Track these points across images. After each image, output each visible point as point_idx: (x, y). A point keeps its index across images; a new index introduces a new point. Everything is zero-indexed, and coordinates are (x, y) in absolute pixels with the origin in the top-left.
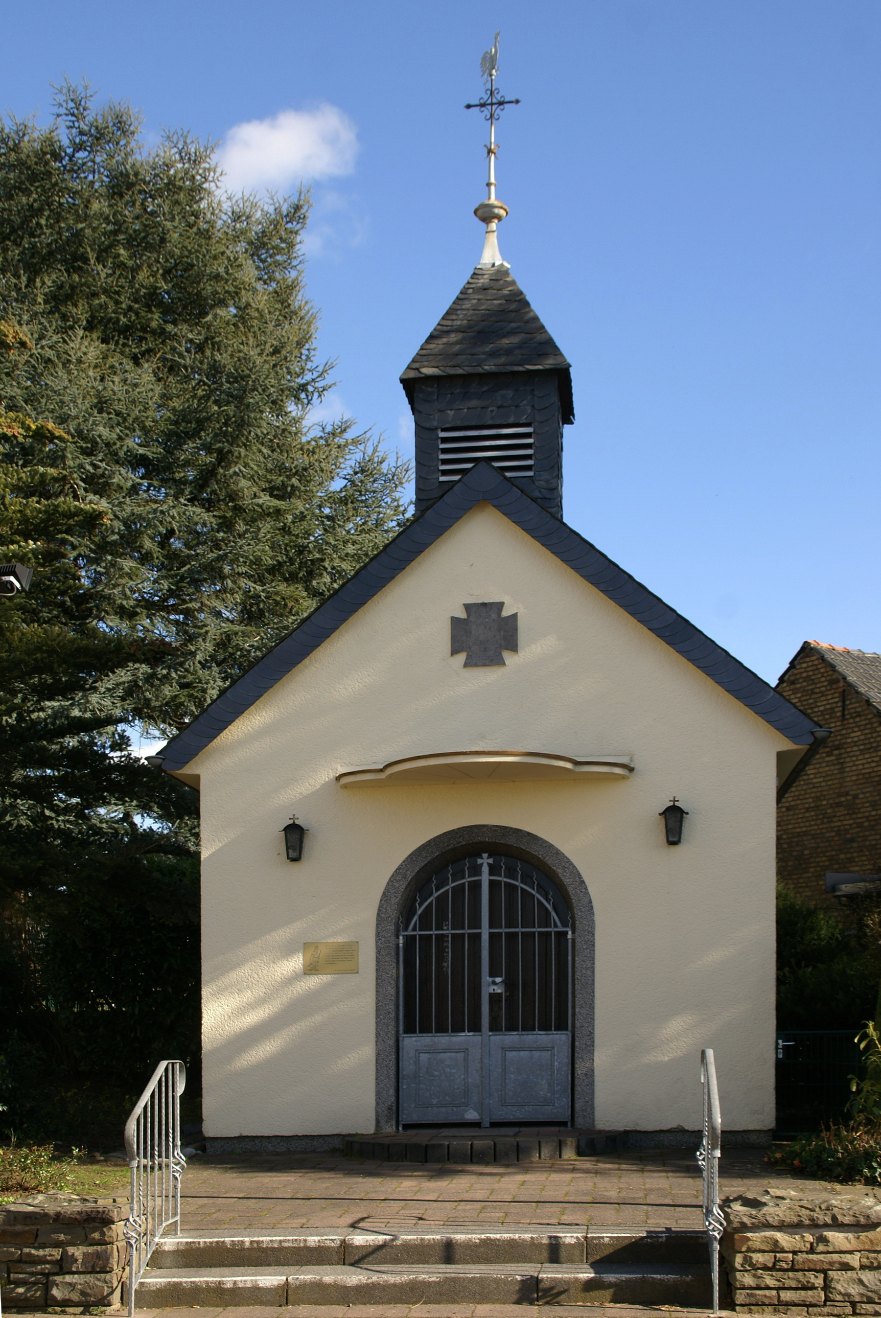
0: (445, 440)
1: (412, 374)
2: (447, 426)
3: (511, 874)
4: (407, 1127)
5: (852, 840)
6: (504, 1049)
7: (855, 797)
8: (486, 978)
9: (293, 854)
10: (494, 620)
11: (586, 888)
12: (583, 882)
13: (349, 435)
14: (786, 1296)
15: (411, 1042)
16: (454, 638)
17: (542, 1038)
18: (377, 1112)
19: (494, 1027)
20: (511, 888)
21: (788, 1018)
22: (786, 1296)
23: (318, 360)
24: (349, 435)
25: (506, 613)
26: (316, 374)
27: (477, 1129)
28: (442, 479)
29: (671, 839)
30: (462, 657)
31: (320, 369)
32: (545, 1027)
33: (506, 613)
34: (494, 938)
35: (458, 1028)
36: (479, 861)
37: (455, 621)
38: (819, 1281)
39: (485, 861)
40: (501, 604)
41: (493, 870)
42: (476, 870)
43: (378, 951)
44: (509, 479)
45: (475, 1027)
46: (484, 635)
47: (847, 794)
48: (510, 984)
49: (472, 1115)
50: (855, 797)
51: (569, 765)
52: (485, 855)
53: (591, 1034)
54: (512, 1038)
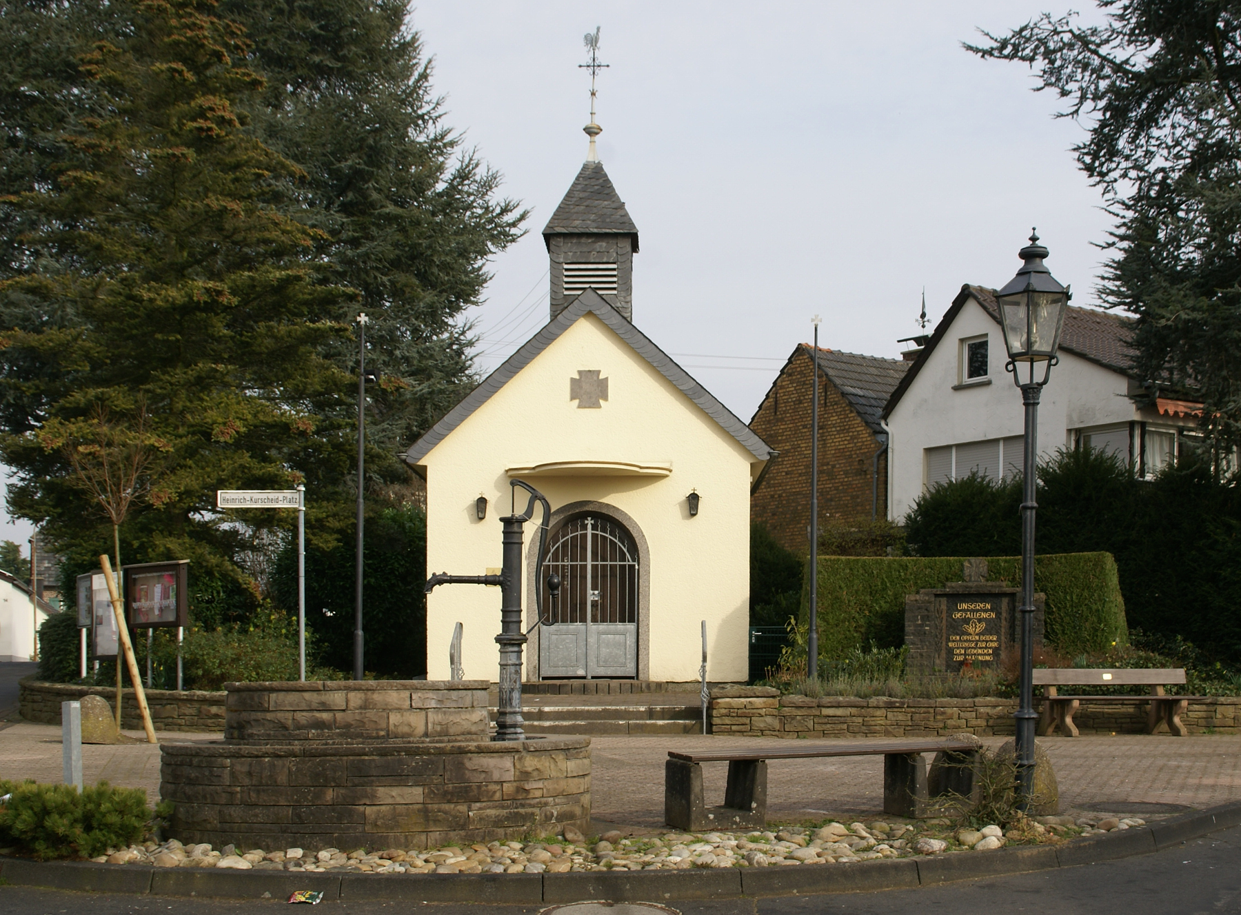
0: (567, 270)
1: (549, 231)
3: (604, 530)
4: (544, 678)
5: (831, 500)
6: (599, 633)
7: (834, 466)
8: (590, 592)
13: (447, 139)
14: (734, 728)
16: (572, 390)
17: (620, 626)
19: (594, 620)
20: (604, 538)
21: (756, 619)
22: (734, 728)
23: (432, 96)
24: (447, 139)
25: (601, 377)
26: (432, 106)
28: (566, 293)
30: (576, 402)
31: (435, 101)
32: (622, 620)
33: (601, 377)
34: (594, 568)
35: (573, 620)
37: (573, 380)
38: (748, 721)
39: (589, 522)
41: (594, 527)
42: (584, 527)
44: (600, 296)
45: (583, 620)
46: (589, 390)
47: (828, 464)
48: (603, 596)
49: (581, 672)
50: (834, 466)
53: (648, 625)
54: (603, 627)
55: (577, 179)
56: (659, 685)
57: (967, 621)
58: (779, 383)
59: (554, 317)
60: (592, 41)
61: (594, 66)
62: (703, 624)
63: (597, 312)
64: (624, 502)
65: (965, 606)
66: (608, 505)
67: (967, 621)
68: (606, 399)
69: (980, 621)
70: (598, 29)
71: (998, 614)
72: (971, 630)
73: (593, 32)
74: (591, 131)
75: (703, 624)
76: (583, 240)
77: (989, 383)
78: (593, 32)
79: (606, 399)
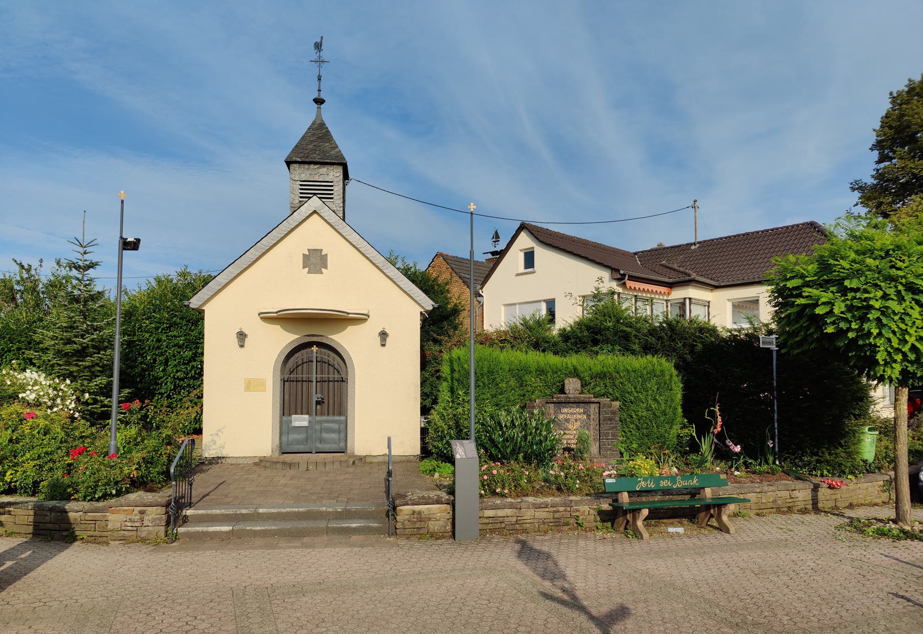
55: (309, 129)
56: (362, 459)
57: (567, 420)
59: (726, 504)
60: (318, 46)
62: (389, 439)
64: (343, 339)
65: (565, 410)
67: (567, 420)
68: (326, 268)
69: (576, 420)
71: (589, 416)
72: (570, 427)
73: (319, 41)
74: (319, 101)
75: (389, 439)
76: (312, 166)
77: (534, 272)
78: (319, 41)
79: (326, 268)
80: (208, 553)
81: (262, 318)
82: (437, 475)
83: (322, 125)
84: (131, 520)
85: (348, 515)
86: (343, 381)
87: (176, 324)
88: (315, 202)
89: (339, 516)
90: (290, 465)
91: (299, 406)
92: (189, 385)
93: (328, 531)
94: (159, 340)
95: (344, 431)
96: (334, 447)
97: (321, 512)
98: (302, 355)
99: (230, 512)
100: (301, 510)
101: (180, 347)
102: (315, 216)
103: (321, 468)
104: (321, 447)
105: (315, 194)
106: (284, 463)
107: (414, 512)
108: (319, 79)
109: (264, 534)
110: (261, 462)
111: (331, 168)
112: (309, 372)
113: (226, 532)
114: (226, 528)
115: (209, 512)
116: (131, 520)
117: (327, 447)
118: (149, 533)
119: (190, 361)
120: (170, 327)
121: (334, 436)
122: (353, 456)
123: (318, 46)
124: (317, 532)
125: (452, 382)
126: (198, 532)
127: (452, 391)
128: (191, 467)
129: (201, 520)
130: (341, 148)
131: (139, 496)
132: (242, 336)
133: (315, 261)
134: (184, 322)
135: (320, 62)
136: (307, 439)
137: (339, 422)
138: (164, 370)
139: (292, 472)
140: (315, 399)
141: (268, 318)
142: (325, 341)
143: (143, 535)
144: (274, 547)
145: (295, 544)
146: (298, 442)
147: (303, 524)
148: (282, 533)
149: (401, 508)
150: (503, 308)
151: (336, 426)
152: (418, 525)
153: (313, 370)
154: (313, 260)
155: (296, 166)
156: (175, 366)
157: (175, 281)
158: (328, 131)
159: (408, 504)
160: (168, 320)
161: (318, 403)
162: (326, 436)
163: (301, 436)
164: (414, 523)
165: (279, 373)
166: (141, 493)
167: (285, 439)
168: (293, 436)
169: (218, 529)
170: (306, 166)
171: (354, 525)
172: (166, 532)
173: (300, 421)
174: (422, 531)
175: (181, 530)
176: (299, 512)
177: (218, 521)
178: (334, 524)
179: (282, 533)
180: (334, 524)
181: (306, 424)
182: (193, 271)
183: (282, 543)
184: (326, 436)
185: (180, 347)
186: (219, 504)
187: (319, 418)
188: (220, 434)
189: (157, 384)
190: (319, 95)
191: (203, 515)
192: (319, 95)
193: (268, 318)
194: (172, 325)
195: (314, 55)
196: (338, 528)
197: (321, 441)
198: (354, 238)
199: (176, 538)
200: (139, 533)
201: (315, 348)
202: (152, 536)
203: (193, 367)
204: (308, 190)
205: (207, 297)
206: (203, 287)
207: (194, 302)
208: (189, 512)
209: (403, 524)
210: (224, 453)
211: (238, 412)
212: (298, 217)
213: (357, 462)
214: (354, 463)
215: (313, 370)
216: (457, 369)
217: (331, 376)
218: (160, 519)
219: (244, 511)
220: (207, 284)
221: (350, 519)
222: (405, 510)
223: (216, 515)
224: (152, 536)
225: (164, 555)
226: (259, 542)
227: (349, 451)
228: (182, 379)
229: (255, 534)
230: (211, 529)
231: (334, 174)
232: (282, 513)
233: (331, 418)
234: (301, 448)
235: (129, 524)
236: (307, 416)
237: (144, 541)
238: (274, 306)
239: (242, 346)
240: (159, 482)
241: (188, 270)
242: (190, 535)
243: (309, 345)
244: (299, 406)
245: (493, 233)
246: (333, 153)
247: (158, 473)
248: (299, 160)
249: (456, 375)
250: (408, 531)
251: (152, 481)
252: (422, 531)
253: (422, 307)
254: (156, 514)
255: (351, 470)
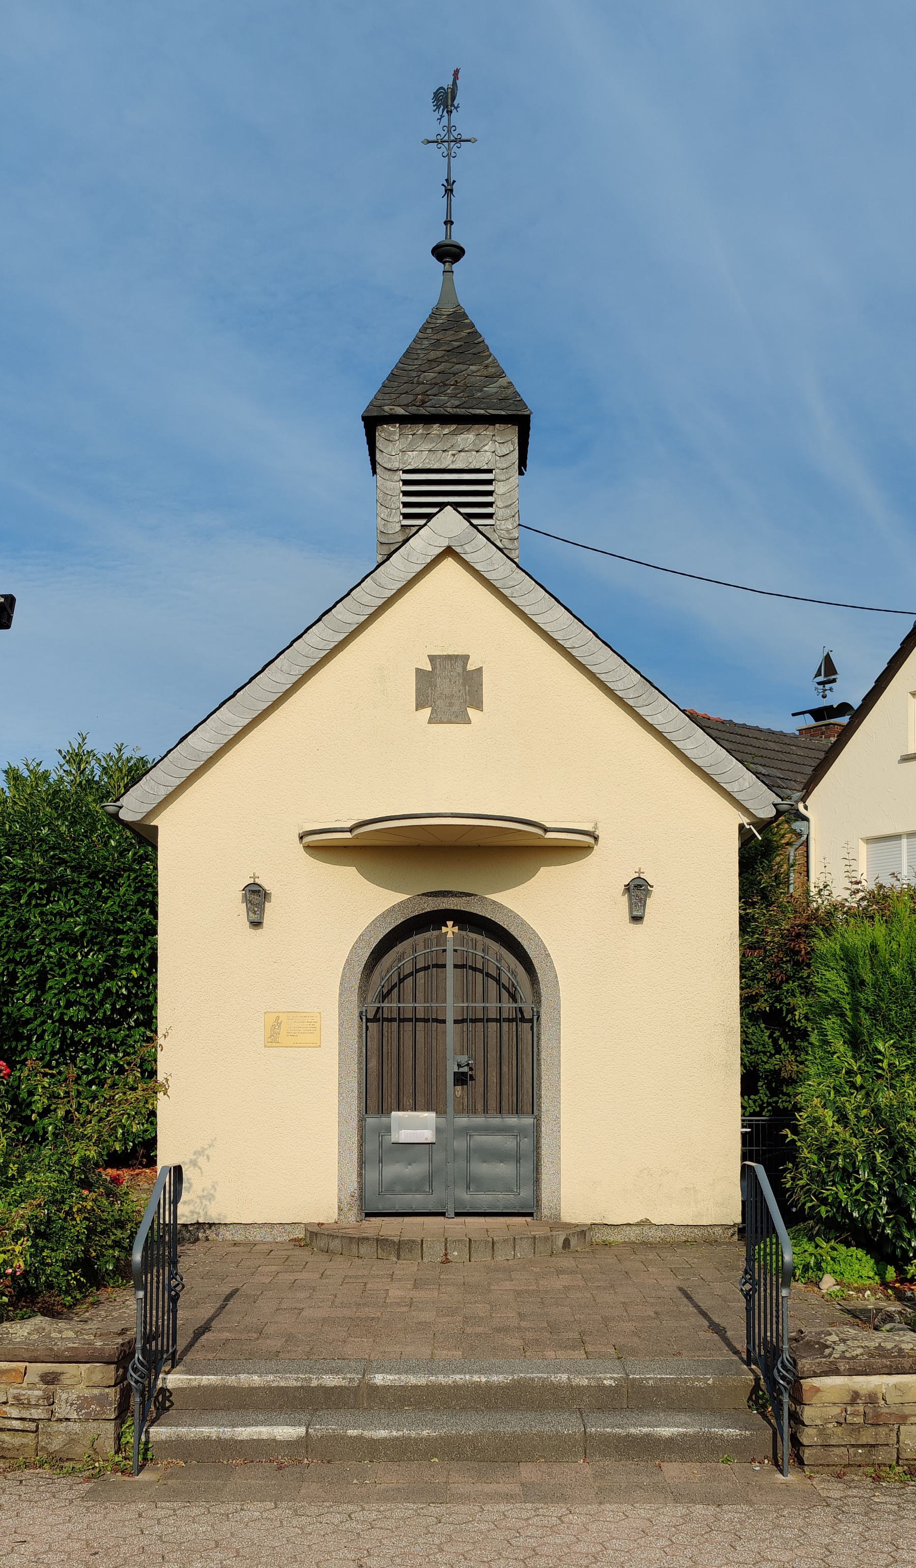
2: (409, 467)
9: (254, 917)
10: (459, 674)
11: (551, 962)
12: (548, 955)
15: (371, 1121)
18: (339, 1199)
27: (442, 1218)
29: (635, 913)
36: (444, 929)
40: (467, 657)
43: (341, 1025)
51: (540, 832)
52: (450, 923)
55: (423, 329)
56: (583, 1231)
58: (148, 916)
60: (445, 99)
61: (451, 141)
62: (794, 715)
63: (458, 550)
64: (530, 903)
66: (502, 907)
68: (479, 706)
70: (456, 73)
74: (448, 253)
75: (794, 715)
76: (436, 429)
78: (447, 82)
79: (479, 706)
80: (254, 1510)
81: (309, 848)
82: (828, 1283)
83: (458, 319)
84: (19, 1402)
85: (634, 1398)
86: (533, 1020)
87: (64, 881)
88: (448, 525)
89: (608, 1401)
90: (399, 1247)
91: (408, 1089)
92: (97, 1041)
93: (588, 1446)
94: (22, 925)
95: (531, 1157)
96: (502, 1199)
97: (555, 1389)
98: (416, 947)
99: (291, 1381)
100: (496, 1378)
101: (76, 941)
102: (449, 562)
103: (482, 1257)
104: (469, 1198)
105: (442, 506)
106: (381, 1242)
107: (855, 1396)
108: (449, 191)
109: (399, 1451)
110: (314, 1238)
111: (487, 431)
112: (436, 992)
113: (289, 1444)
114: (286, 1432)
115: (231, 1380)
116: (19, 1402)
117: (484, 1200)
118: (72, 1441)
119: (99, 979)
120: (48, 891)
121: (505, 1169)
122: (557, 1224)
123: (445, 99)
124: (557, 1450)
125: (856, 1016)
126: (207, 1441)
127: (855, 1042)
128: (171, 1240)
129: (210, 1403)
130: (512, 376)
131: (38, 1330)
132: (256, 896)
133: (450, 688)
134: (83, 879)
135: (451, 141)
136: (430, 1178)
137: (518, 1132)
138: (36, 1002)
139: (407, 1267)
140: (452, 1068)
141: (325, 847)
142: (476, 909)
143: (56, 1445)
144: (437, 1495)
145: (502, 1488)
146: (410, 1186)
147: (512, 1424)
148: (452, 1450)
149: (817, 1382)
150: (863, 848)
151: (508, 1143)
152: (867, 1437)
153: (447, 990)
154: (443, 685)
155: (393, 429)
156: (64, 990)
157: (53, 777)
158: (476, 334)
159: (836, 1372)
160: (42, 871)
161: (461, 1079)
162: (482, 1169)
163: (416, 1170)
164: (855, 1429)
165: (355, 997)
166: (39, 1320)
167: (372, 1175)
168: (393, 1170)
169: (263, 1432)
170: (420, 429)
171: (666, 1432)
172: (119, 1438)
173: (414, 1126)
174: (881, 1456)
175: (159, 1433)
176: (489, 1386)
177: (227, 1408)
178: (604, 1427)
179: (452, 1450)
180: (604, 1427)
181: (428, 1135)
182: (102, 746)
183: (462, 1483)
184: (482, 1169)
185: (76, 941)
186: (252, 1359)
187: (463, 1121)
188: (201, 1161)
189: (19, 1037)
190: (448, 234)
191: (212, 1390)
192: (448, 234)
193: (325, 847)
194: (54, 886)
195: (431, 123)
196: (618, 1438)
197: (470, 1182)
198: (556, 619)
199: (146, 1457)
200: (43, 1441)
201: (450, 929)
202: (81, 1450)
203: (108, 992)
204: (425, 496)
205: (163, 792)
206: (127, 788)
207: (132, 807)
208: (173, 1380)
209: (822, 1431)
210: (213, 1215)
211: (251, 1096)
212: (400, 567)
213: (573, 1242)
214: (567, 1243)
215: (447, 990)
216: (868, 977)
217: (493, 1005)
218: (101, 1400)
219: (330, 1380)
220: (135, 781)
221: (641, 1410)
222: (827, 1392)
223: (252, 1390)
224: (81, 1450)
225: (128, 1513)
226: (389, 1476)
227: (545, 1212)
228: (81, 1025)
229: (373, 1450)
230: (245, 1433)
231: (490, 449)
232: (441, 1388)
233: (496, 1121)
234: (416, 1201)
235: (15, 1413)
236: (430, 1116)
237: (57, 1462)
238: (343, 812)
239: (256, 924)
240: (67, 1293)
241: (87, 748)
242: (180, 1448)
243: (435, 919)
244: (408, 1089)
245: (818, 660)
246: (491, 389)
247: (68, 1265)
248: (400, 411)
249: (868, 997)
250: (838, 1455)
251: (50, 1286)
252: (881, 1456)
253: (746, 811)
254: (86, 1382)
255: (567, 1262)
